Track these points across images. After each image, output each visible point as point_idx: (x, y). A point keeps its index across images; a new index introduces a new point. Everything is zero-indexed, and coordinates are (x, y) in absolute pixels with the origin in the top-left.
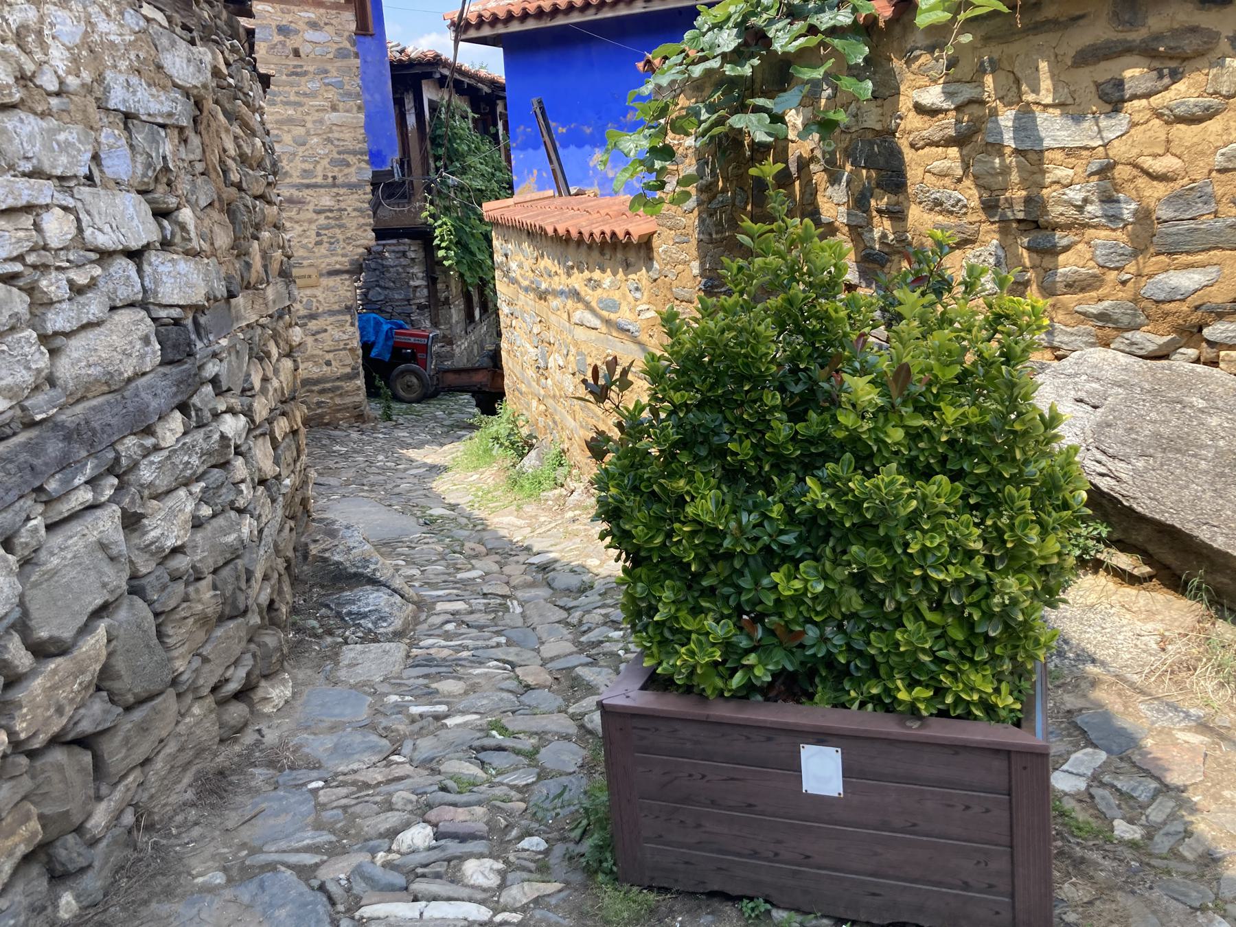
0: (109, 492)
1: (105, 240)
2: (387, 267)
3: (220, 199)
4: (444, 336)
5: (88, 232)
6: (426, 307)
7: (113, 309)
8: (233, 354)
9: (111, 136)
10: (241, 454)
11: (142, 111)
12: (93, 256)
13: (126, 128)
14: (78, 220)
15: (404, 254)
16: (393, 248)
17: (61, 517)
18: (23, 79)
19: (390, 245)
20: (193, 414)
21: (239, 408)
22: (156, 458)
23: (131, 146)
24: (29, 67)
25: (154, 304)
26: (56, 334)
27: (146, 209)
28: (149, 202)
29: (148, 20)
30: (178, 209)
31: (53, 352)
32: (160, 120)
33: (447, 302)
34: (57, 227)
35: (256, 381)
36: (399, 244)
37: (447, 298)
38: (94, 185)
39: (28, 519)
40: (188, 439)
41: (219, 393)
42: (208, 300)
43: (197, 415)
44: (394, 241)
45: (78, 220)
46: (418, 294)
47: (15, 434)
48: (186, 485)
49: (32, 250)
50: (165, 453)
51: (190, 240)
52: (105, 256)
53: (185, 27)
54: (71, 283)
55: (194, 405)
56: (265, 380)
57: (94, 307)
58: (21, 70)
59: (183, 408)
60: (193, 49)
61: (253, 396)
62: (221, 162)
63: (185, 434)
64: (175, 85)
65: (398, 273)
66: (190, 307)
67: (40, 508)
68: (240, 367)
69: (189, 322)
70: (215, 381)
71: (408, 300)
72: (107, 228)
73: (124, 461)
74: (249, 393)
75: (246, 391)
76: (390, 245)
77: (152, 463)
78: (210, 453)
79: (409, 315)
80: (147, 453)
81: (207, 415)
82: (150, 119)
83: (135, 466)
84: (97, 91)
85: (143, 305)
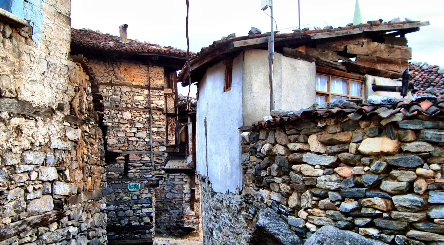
0: (34, 239)
1: (44, 179)
2: (175, 184)
3: (80, 167)
4: (196, 214)
5: (40, 177)
7: (43, 195)
8: (77, 210)
9: (50, 155)
10: (75, 239)
12: (41, 182)
13: (54, 152)
14: (38, 174)
15: (182, 180)
16: (178, 177)
18: (32, 144)
21: (76, 225)
22: (48, 233)
23: (55, 156)
24: (33, 141)
26: (29, 200)
27: (56, 170)
28: (56, 169)
29: (65, 125)
31: (27, 204)
34: (34, 176)
35: (84, 219)
36: (180, 175)
37: (199, 198)
38: (44, 166)
39: (15, 241)
40: (58, 231)
41: (69, 219)
42: (70, 194)
45: (38, 174)
46: (186, 196)
47: (16, 221)
49: (27, 180)
52: (43, 182)
53: (75, 125)
54: (34, 188)
56: (88, 218)
57: (39, 193)
58: (32, 142)
59: (58, 222)
60: (76, 130)
62: (82, 156)
64: (69, 140)
65: (179, 187)
66: (64, 196)
67: (18, 239)
68: (78, 214)
70: (69, 216)
72: (45, 176)
73: (40, 233)
75: (80, 220)
78: (63, 236)
79: (181, 205)
80: (46, 232)
81: (65, 225)
83: (42, 234)
84: (48, 145)
85: (52, 194)
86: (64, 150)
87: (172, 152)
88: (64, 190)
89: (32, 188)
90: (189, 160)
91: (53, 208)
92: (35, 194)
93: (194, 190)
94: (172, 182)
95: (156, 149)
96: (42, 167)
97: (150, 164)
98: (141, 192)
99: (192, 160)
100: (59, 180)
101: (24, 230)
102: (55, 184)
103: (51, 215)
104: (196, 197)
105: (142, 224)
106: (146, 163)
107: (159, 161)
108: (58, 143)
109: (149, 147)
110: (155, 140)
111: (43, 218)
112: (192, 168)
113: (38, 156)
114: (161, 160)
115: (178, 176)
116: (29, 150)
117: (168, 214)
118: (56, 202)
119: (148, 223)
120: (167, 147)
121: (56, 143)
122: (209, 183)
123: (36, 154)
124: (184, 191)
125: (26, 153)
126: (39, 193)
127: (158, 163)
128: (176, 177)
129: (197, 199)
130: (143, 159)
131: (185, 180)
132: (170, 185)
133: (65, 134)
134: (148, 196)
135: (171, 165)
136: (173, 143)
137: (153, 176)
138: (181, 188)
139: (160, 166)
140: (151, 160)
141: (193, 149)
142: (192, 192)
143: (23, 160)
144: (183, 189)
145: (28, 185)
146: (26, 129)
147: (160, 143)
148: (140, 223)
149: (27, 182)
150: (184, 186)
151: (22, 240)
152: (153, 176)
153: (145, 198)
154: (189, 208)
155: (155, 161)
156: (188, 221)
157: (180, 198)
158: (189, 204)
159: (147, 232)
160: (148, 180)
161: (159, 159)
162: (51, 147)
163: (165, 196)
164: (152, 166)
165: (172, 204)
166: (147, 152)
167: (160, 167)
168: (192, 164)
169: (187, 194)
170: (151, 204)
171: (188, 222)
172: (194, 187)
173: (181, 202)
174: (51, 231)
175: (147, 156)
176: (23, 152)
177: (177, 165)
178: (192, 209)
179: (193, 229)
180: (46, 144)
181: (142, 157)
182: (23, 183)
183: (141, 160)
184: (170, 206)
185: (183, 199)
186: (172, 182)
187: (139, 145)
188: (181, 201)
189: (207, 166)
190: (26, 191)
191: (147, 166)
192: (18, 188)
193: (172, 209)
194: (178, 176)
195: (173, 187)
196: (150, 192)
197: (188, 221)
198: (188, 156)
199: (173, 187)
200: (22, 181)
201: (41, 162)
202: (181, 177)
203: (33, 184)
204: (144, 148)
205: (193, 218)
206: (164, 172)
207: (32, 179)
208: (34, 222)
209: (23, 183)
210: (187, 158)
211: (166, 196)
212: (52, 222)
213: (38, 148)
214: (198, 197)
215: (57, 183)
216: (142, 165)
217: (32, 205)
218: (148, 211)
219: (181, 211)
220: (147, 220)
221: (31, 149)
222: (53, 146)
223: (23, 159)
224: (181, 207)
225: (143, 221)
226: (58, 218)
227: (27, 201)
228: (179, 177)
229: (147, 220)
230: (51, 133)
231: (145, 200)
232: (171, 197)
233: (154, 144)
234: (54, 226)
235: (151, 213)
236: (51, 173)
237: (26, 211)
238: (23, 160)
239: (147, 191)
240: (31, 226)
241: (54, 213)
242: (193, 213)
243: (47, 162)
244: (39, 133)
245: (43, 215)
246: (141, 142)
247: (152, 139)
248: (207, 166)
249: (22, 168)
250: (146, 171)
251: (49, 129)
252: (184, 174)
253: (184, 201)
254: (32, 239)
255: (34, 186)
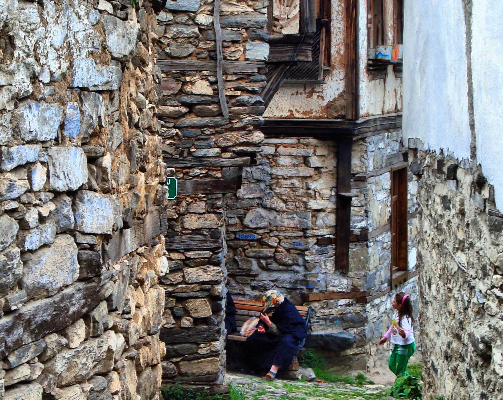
1: (60, 185)
2: (277, 178)
4: (355, 289)
6: (329, 241)
11: (91, 85)
14: (48, 172)
15: (306, 160)
16: (289, 150)
17: (13, 383)
18: (34, 78)
19: (286, 146)
20: (92, 325)
22: (67, 354)
25: (79, 232)
27: (84, 158)
29: (101, 11)
30: (103, 155)
32: (100, 89)
33: (363, 237)
36: (297, 145)
37: (364, 230)
40: (87, 345)
41: (111, 310)
43: (94, 326)
44: (292, 140)
45: (48, 172)
46: (320, 222)
48: (80, 383)
50: (72, 352)
51: (107, 181)
52: (57, 194)
54: (40, 214)
55: (94, 317)
57: (50, 228)
61: (129, 319)
63: (86, 340)
64: (113, 58)
65: (293, 188)
69: (99, 248)
70: (109, 300)
71: (304, 230)
74: (127, 316)
76: (286, 146)
77: (64, 358)
79: (302, 253)
82: (95, 89)
86: (100, 92)
87: (286, 63)
88: (104, 218)
89: (36, 216)
90: (333, 86)
91: (77, 276)
92: (42, 232)
93: (350, 199)
94: (268, 169)
95: (237, 52)
96: (54, 148)
97: (213, 108)
98: (182, 210)
99: (342, 89)
100: (91, 189)
101: (18, 344)
102: (82, 200)
103: (72, 296)
104: (357, 224)
105: (186, 322)
106: (199, 103)
107: (245, 97)
108: (88, 70)
109: (210, 45)
110: (233, 19)
111: (56, 306)
112: (343, 117)
113: (47, 114)
114: (253, 92)
115: (291, 145)
116: (27, 97)
117: (254, 288)
118: (85, 256)
119: (205, 321)
120: (272, 43)
121: (88, 73)
122: (480, 183)
123: (44, 111)
124: (313, 204)
125: (22, 109)
126: (50, 228)
127: (242, 104)
128: (281, 149)
129: (357, 232)
130: (188, 88)
131: (315, 162)
132: (259, 181)
133: (104, 40)
134: (207, 224)
135: (284, 105)
136: (292, 29)
137: (224, 150)
138: (301, 192)
139: (249, 114)
140: (216, 92)
141: (347, 46)
142: (343, 205)
143: (16, 131)
144: (310, 196)
145: (28, 205)
146: (22, 34)
147: (247, 29)
148: (178, 318)
149: (24, 199)
150: (313, 185)
151: (11, 374)
152: (224, 150)
153: (197, 231)
154: (330, 266)
155: (231, 97)
156: (326, 311)
157: (295, 229)
158: (331, 249)
159: (201, 352)
160: (205, 166)
161: (244, 90)
162: (75, 85)
163: (241, 219)
164: (221, 114)
165: (267, 252)
166: (203, 63)
167: (248, 119)
168: (342, 102)
169: (322, 215)
170: (215, 250)
171: (326, 318)
172: (348, 190)
173: (301, 244)
174: (72, 345)
175: (205, 78)
176: (16, 107)
177: (288, 107)
178: (342, 267)
179: (346, 344)
180: (64, 76)
181: (185, 83)
182: (14, 200)
183: (181, 92)
184: (258, 258)
185: (309, 233)
186: (268, 169)
187: (174, 38)
188: (302, 241)
189: (472, 127)
190: (24, 226)
191: (201, 114)
192: (6, 216)
193: (266, 269)
194: (291, 145)
195: (270, 187)
196: (213, 209)
197: (326, 311)
198: (327, 72)
199: (270, 187)
200: (15, 194)
201: (54, 135)
202: (302, 151)
203: (37, 202)
204: (192, 49)
205: (342, 302)
206: (262, 135)
207: (36, 188)
208: (38, 319)
209: (14, 200)
210: (323, 82)
211: (246, 221)
212: (75, 318)
213: (46, 91)
214: (363, 224)
215: (88, 195)
216: (184, 110)
217: (33, 269)
218: (206, 278)
219: (300, 277)
220: (202, 308)
221: (32, 97)
222: (77, 83)
223: (17, 127)
224: (300, 261)
225: (187, 312)
226: (89, 306)
227: (25, 254)
228: (294, 151)
229: (202, 308)
230: (73, 41)
231: (198, 237)
232: (264, 224)
233: (229, 34)
234: (80, 330)
235: (217, 283)
236: (72, 166)
237: (21, 288)
238: (16, 131)
239: (201, 206)
240: (32, 332)
241: (79, 290)
242: (342, 283)
243: (65, 133)
244: (48, 42)
245: (57, 298)
246: (181, 28)
247: (222, 14)
248: (472, 127)
249: (15, 156)
250: (198, 132)
251: (69, 29)
252: (312, 141)
253: (312, 241)
254: (33, 372)
255: (40, 209)
